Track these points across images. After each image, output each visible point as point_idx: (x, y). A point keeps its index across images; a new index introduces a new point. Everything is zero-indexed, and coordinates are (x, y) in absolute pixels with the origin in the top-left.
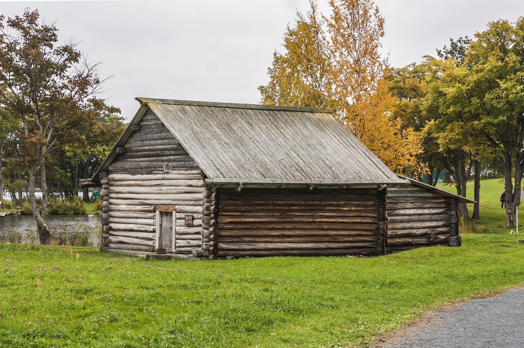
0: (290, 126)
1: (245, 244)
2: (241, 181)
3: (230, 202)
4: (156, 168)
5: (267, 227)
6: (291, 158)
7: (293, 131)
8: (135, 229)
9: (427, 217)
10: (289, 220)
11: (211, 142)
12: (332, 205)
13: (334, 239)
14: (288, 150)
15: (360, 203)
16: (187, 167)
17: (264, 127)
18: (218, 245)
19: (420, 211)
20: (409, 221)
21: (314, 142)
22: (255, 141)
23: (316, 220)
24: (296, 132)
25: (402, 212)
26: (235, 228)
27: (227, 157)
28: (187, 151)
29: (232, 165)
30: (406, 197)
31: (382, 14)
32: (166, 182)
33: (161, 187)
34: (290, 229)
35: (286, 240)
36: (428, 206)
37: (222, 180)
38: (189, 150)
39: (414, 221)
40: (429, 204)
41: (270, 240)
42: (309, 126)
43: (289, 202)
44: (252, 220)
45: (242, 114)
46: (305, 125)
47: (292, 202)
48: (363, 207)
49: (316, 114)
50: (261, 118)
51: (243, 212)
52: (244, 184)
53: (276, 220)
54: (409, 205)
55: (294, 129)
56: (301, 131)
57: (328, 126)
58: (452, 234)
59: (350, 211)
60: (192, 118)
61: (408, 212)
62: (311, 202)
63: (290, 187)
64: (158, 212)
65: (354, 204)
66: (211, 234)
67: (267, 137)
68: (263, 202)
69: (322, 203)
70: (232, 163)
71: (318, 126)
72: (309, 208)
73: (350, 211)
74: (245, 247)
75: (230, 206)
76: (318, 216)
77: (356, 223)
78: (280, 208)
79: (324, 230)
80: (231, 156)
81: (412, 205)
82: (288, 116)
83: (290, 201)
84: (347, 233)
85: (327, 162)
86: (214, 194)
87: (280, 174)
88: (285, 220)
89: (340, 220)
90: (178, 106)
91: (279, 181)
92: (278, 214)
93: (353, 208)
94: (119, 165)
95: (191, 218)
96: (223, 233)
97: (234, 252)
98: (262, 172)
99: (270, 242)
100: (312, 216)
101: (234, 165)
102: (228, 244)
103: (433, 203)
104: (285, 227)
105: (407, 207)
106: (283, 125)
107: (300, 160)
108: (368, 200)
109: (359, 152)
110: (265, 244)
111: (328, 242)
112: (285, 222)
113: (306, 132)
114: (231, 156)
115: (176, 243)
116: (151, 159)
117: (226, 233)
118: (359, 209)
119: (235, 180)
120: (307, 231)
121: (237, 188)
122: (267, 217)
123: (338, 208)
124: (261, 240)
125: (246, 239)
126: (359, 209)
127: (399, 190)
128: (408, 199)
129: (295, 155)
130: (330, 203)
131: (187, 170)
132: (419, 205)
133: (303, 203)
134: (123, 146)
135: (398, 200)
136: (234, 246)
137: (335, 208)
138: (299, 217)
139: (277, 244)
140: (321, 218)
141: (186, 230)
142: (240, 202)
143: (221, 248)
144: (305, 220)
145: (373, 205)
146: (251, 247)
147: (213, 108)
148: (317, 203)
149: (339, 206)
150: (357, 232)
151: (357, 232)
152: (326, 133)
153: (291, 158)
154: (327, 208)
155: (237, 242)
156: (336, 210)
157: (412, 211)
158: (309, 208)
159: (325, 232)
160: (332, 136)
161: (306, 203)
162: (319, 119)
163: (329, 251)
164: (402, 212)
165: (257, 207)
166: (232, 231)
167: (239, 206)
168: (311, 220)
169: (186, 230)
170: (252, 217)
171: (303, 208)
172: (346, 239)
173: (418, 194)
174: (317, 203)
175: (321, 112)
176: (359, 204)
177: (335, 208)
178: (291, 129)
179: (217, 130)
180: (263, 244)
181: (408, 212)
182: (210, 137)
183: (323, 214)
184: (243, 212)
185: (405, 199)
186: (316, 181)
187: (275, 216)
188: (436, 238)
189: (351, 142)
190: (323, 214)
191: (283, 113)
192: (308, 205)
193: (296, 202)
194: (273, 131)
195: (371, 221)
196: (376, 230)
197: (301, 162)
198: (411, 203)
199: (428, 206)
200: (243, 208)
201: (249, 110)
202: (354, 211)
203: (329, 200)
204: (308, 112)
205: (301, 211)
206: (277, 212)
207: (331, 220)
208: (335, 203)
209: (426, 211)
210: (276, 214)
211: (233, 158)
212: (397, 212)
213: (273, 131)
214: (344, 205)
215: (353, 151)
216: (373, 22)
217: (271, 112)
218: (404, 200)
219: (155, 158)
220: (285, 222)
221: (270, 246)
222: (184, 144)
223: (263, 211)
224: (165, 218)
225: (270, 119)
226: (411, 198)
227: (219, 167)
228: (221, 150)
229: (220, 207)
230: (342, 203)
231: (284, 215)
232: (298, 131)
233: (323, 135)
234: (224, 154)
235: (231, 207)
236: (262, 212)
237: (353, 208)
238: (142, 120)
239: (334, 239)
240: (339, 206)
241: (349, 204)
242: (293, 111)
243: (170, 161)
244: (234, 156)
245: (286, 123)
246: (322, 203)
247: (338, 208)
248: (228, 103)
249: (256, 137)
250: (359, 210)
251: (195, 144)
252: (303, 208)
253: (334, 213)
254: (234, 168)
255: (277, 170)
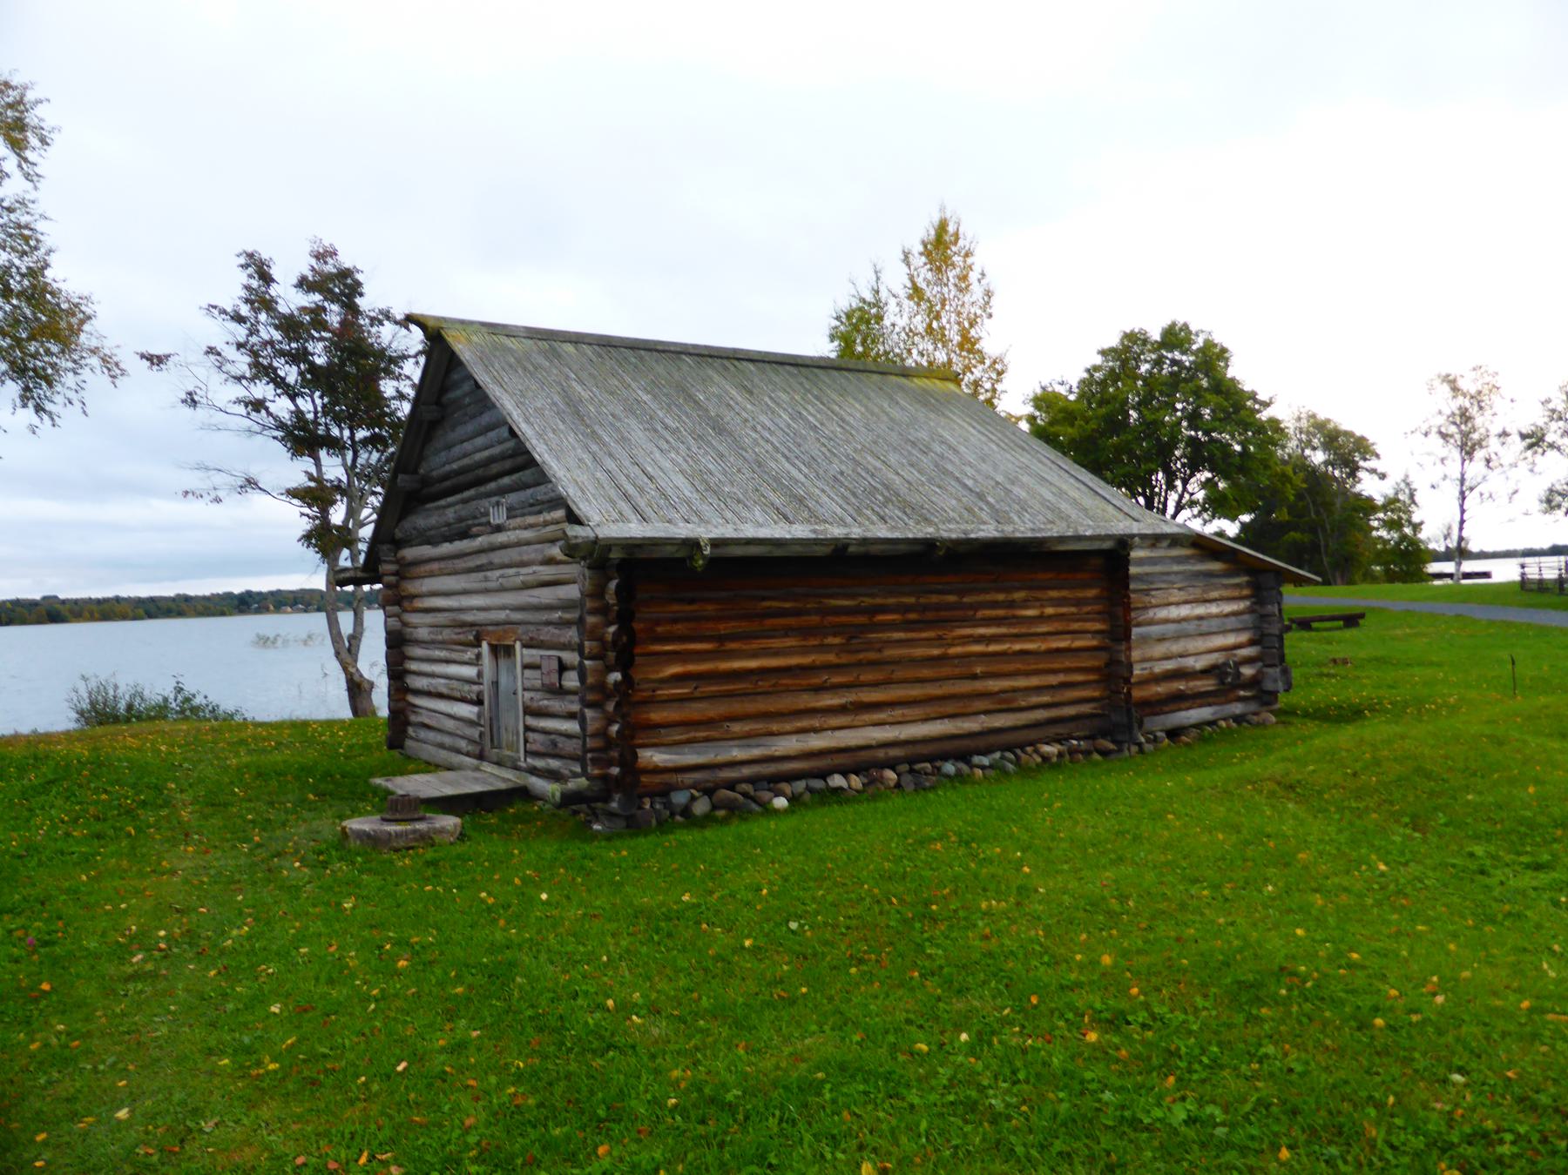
0: (855, 399)
1: (736, 742)
2: (704, 533)
3: (676, 607)
4: (475, 518)
5: (804, 682)
6: (868, 471)
7: (863, 410)
8: (445, 691)
9: (1214, 623)
10: (872, 656)
11: (618, 424)
12: (995, 605)
13: (1003, 701)
14: (855, 450)
15: (1064, 593)
16: (543, 503)
17: (784, 396)
18: (635, 756)
19: (1200, 610)
20: (1177, 637)
21: (923, 435)
22: (759, 428)
23: (953, 651)
24: (872, 414)
25: (1162, 613)
26: (697, 694)
27: (667, 465)
28: (527, 445)
29: (680, 484)
30: (1168, 574)
31: (993, 280)
32: (497, 557)
33: (489, 574)
34: (875, 685)
35: (867, 717)
36: (1215, 594)
37: (635, 529)
38: (534, 442)
39: (1188, 636)
40: (1217, 589)
41: (816, 723)
42: (902, 402)
43: (868, 601)
44: (753, 664)
45: (726, 369)
46: (892, 399)
47: (878, 601)
48: (1073, 605)
49: (915, 380)
50: (776, 379)
51: (721, 639)
52: (716, 543)
53: (831, 658)
54: (1177, 595)
55: (866, 407)
56: (884, 412)
57: (949, 402)
58: (1268, 662)
59: (1041, 618)
60: (575, 367)
61: (1175, 612)
62: (934, 599)
63: (875, 549)
64: (485, 645)
65: (1051, 599)
66: (611, 722)
67: (792, 419)
68: (787, 605)
69: (965, 600)
70: (680, 481)
71: (926, 404)
72: (930, 615)
73: (1041, 618)
74: (738, 754)
75: (675, 621)
76: (954, 638)
77: (1058, 651)
78: (844, 619)
79: (975, 677)
80: (680, 460)
81: (1182, 593)
82: (848, 379)
83: (872, 596)
84: (1034, 681)
85: (970, 483)
86: (613, 585)
87: (839, 511)
88: (861, 656)
89: (1017, 647)
90: (540, 343)
91: (837, 532)
92: (837, 640)
93: (1050, 611)
94: (421, 521)
95: (555, 665)
96: (656, 716)
97: (697, 776)
98: (781, 507)
99: (816, 730)
100: (940, 638)
101: (689, 486)
102: (675, 749)
103: (1226, 587)
104: (862, 678)
105: (1172, 599)
106: (835, 396)
107: (892, 476)
108: (1085, 586)
109: (1041, 462)
110: (801, 737)
111: (986, 712)
112: (859, 664)
113: (895, 413)
114: (680, 460)
115: (526, 741)
116: (467, 494)
117: (665, 714)
118: (1064, 610)
119: (682, 531)
120: (926, 685)
121: (691, 558)
122: (804, 651)
123: (1010, 612)
124: (788, 727)
125: (737, 728)
126: (1064, 610)
127: (1153, 555)
128: (1172, 578)
129: (878, 464)
130: (988, 597)
131: (540, 512)
132: (1196, 592)
133: (912, 600)
134: (415, 472)
135: (1152, 583)
136: (698, 753)
137: (1001, 612)
138: (902, 644)
139: (838, 734)
140: (964, 644)
141: (546, 702)
142: (710, 607)
143: (651, 767)
144: (919, 652)
145: (1096, 599)
146: (756, 752)
147: (642, 352)
148: (952, 598)
149: (1011, 604)
150: (1061, 678)
151: (1061, 678)
152: (948, 418)
153: (868, 471)
154: (980, 614)
155: (707, 740)
156: (1005, 618)
157: (1184, 611)
158: (930, 615)
159: (979, 685)
160: (966, 425)
161: (922, 600)
162: (924, 390)
163: (992, 739)
164: (1162, 613)
165: (769, 622)
166: (687, 704)
167: (708, 619)
168: (936, 652)
169: (546, 702)
170: (754, 655)
171: (913, 616)
172: (1035, 700)
173: (1193, 564)
174: (952, 598)
175: (926, 377)
176: (1065, 598)
177: (1001, 612)
178: (857, 406)
179: (646, 397)
180: (794, 738)
181: (1175, 612)
182: (617, 412)
183: (968, 631)
184: (721, 639)
185: (1165, 578)
186: (950, 530)
187: (828, 645)
188: (1239, 674)
189: (1013, 437)
190: (968, 631)
191: (835, 373)
192: (925, 608)
193: (891, 601)
194: (810, 408)
195: (1094, 643)
196: (1108, 665)
197: (898, 480)
198: (1180, 589)
199: (1215, 594)
200: (724, 628)
201: (745, 363)
202: (1050, 618)
203: (985, 591)
204: (896, 375)
205: (908, 625)
206: (835, 635)
207: (993, 648)
208: (1001, 597)
209: (1214, 609)
210: (830, 640)
211: (685, 466)
212: (1151, 613)
213: (810, 408)
214: (1025, 604)
215: (1025, 459)
216: (977, 292)
217: (803, 370)
218: (1164, 582)
219: (471, 492)
220: (859, 664)
221: (817, 742)
222: (524, 426)
223: (787, 632)
224: (503, 662)
225: (801, 384)
226: (1180, 577)
227: (631, 490)
228: (650, 447)
229: (637, 626)
230: (1019, 595)
231: (854, 641)
232: (876, 410)
233: (943, 421)
234: (657, 455)
235: (679, 626)
236: (786, 635)
237: (1050, 611)
238: (444, 390)
239: (1003, 701)
240: (1011, 604)
241: (1038, 600)
242: (859, 371)
243: (503, 491)
244: (691, 463)
245: (843, 392)
246: (965, 600)
247: (1010, 612)
248: (686, 345)
249: (764, 419)
250: (1062, 615)
251: (562, 427)
252: (913, 616)
253: (999, 625)
254: (687, 493)
255: (827, 499)
